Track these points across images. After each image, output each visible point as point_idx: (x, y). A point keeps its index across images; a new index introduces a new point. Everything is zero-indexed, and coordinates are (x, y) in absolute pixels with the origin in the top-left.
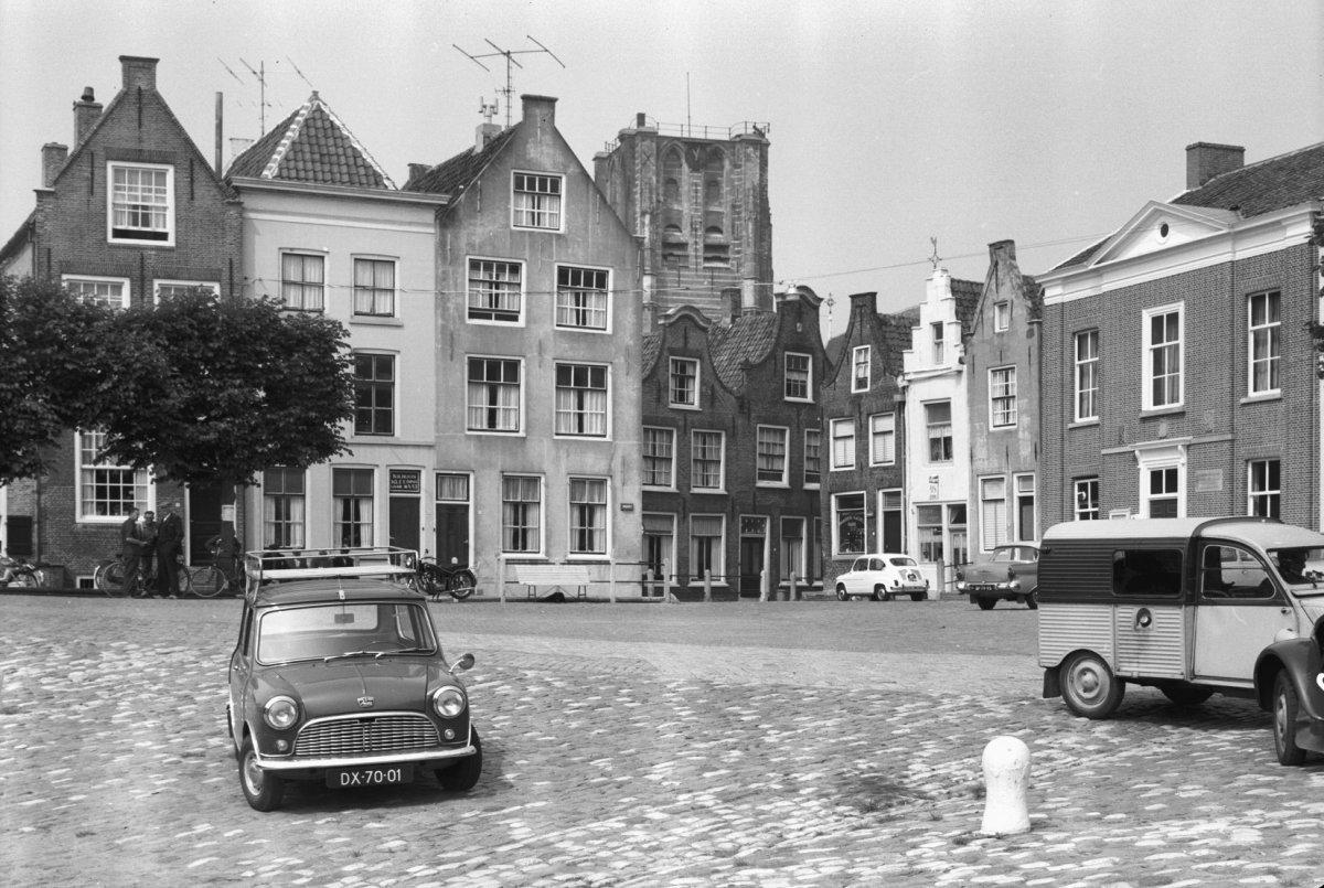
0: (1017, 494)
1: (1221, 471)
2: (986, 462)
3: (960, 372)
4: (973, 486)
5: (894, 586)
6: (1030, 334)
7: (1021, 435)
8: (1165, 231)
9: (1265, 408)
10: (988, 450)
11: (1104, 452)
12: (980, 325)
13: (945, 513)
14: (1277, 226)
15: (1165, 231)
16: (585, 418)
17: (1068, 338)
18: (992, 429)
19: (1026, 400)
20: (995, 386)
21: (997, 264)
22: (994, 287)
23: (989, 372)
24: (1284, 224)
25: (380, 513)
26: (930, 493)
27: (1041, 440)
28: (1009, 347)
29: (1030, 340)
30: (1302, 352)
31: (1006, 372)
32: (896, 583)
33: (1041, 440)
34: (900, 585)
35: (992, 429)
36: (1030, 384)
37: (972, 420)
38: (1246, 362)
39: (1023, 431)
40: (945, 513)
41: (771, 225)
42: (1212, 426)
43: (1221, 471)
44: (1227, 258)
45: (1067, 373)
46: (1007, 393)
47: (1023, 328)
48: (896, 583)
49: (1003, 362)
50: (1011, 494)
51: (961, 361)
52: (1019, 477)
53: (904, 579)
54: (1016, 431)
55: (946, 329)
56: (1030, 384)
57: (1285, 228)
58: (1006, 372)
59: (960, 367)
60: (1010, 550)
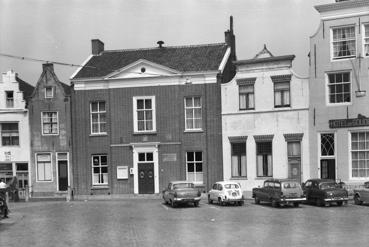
0: (57, 160)
1: (175, 154)
2: (40, 147)
3: (26, 112)
4: (32, 156)
5: (224, 198)
6: (66, 100)
7: (61, 137)
8: (143, 70)
9: (196, 134)
10: (42, 143)
11: (112, 146)
12: (37, 94)
13: (14, 167)
14: (203, 76)
15: (143, 70)
16: (52, 120)
17: (88, 103)
18: (43, 135)
19: (64, 125)
20: (45, 118)
21: (46, 72)
22: (45, 81)
23: (42, 113)
24: (205, 76)
25: (70, 170)
26: (5, 158)
27: (72, 140)
28: (54, 104)
29: (66, 103)
30: (213, 118)
31: (50, 114)
32: (226, 197)
33: (72, 140)
34: (227, 199)
35: (43, 135)
36: (66, 118)
37: (31, 130)
38: (184, 119)
39: (62, 136)
40: (14, 167)
41: (234, 36)
42: (171, 139)
43: (175, 154)
44: (177, 83)
45: (88, 116)
46: (51, 121)
47: (62, 97)
48: (226, 197)
49: (50, 109)
50: (54, 159)
51: (26, 107)
52: (37, 154)
53: (230, 195)
54: (59, 136)
55: (15, 94)
56: (66, 118)
57: (205, 77)
58: (50, 114)
59: (25, 110)
60: (46, 180)
